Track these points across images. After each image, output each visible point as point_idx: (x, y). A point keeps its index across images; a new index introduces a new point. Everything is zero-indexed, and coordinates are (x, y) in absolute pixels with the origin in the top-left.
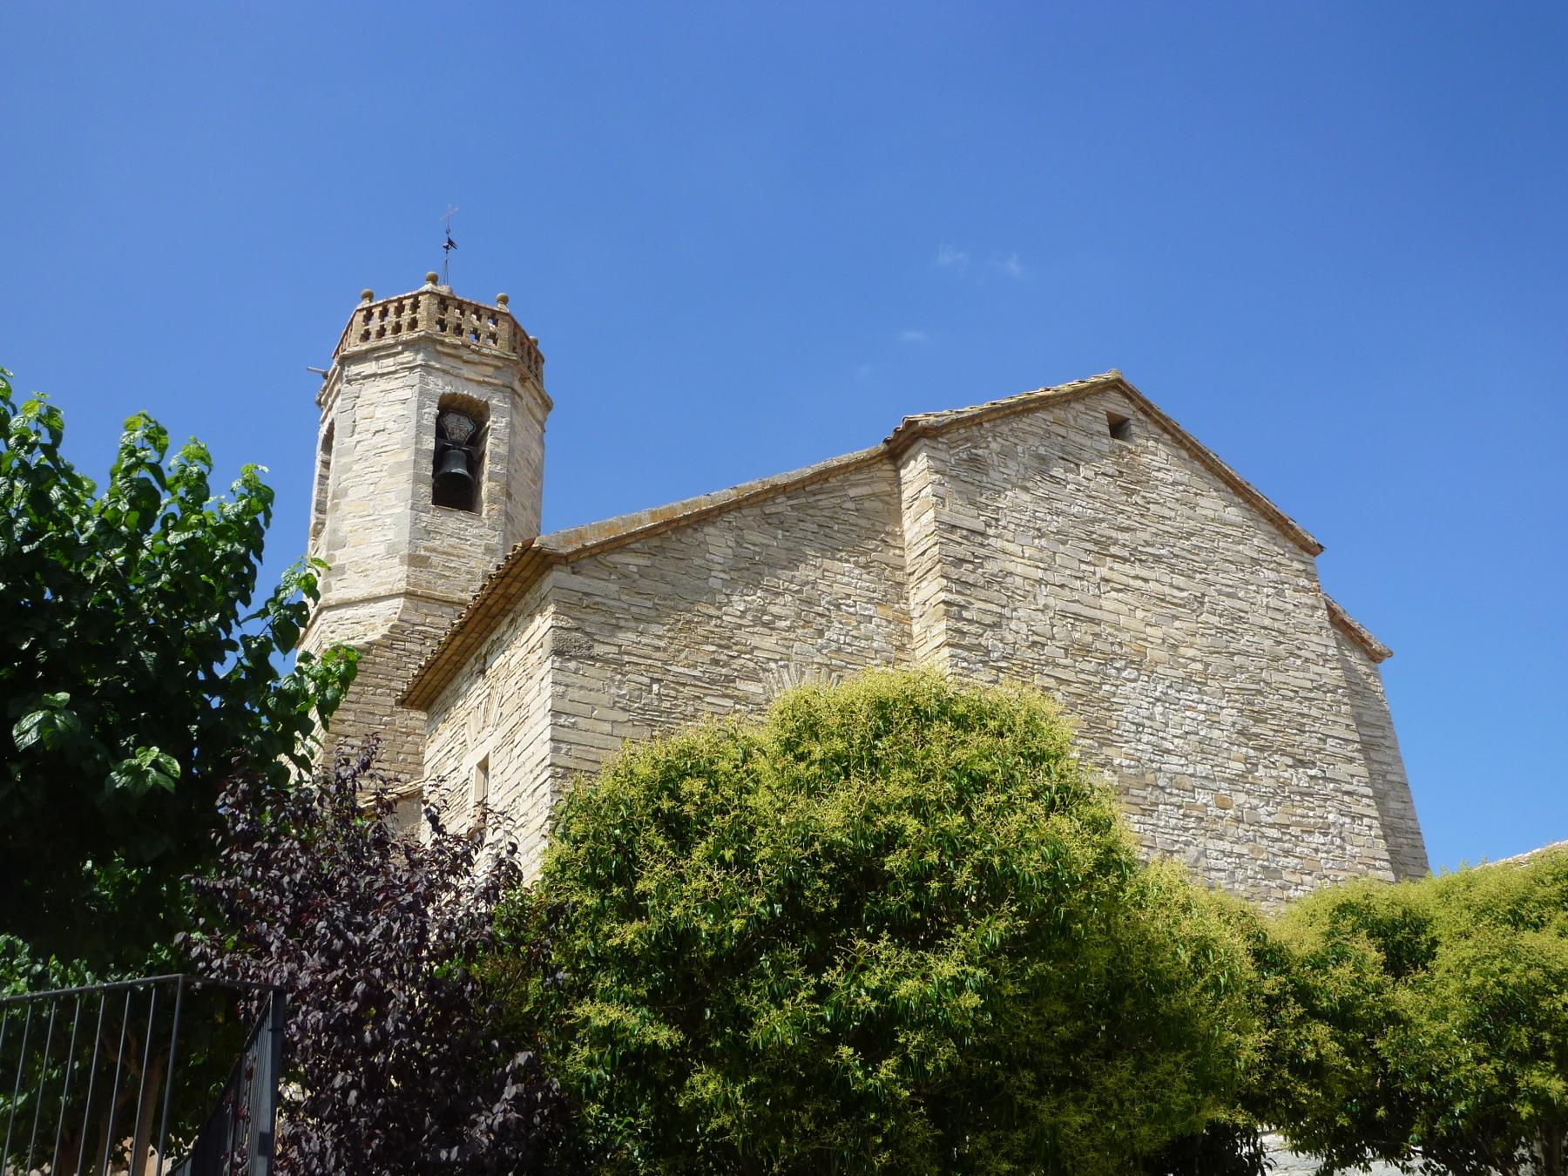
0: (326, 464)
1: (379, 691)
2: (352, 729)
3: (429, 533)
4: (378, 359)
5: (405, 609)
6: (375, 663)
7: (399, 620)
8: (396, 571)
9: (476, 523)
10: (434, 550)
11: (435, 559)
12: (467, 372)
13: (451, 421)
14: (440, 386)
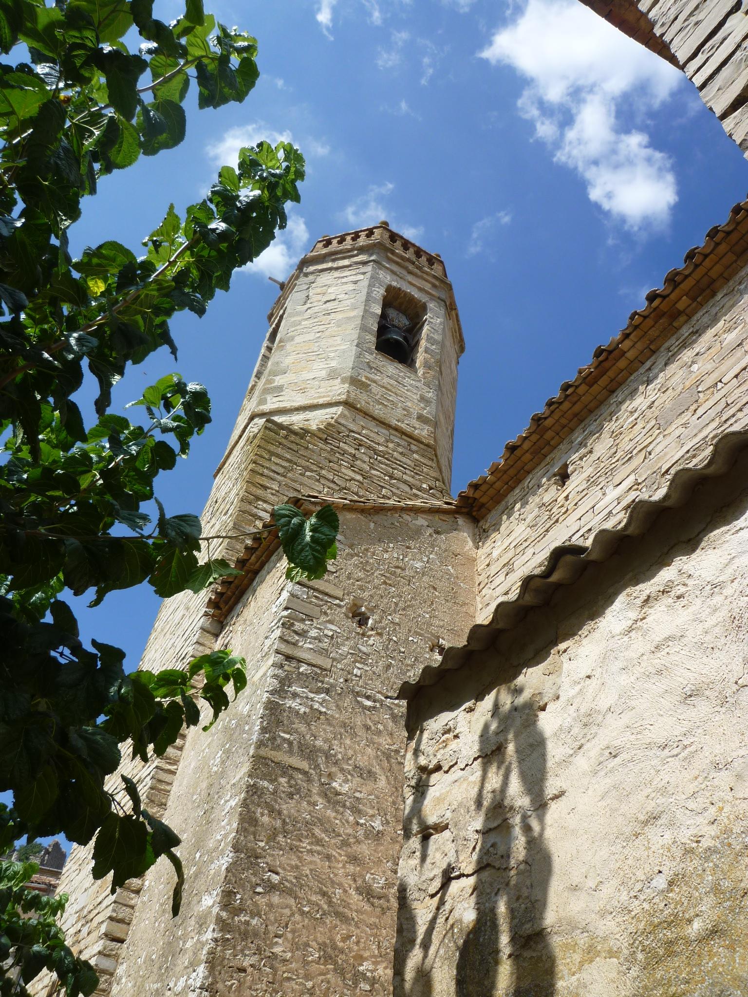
0: (269, 349)
1: (308, 473)
2: (273, 498)
3: (371, 368)
4: (334, 260)
5: (342, 415)
6: (307, 448)
7: (336, 421)
8: (337, 388)
9: (413, 376)
10: (375, 382)
11: (374, 388)
12: (410, 278)
13: (392, 313)
14: (387, 279)
